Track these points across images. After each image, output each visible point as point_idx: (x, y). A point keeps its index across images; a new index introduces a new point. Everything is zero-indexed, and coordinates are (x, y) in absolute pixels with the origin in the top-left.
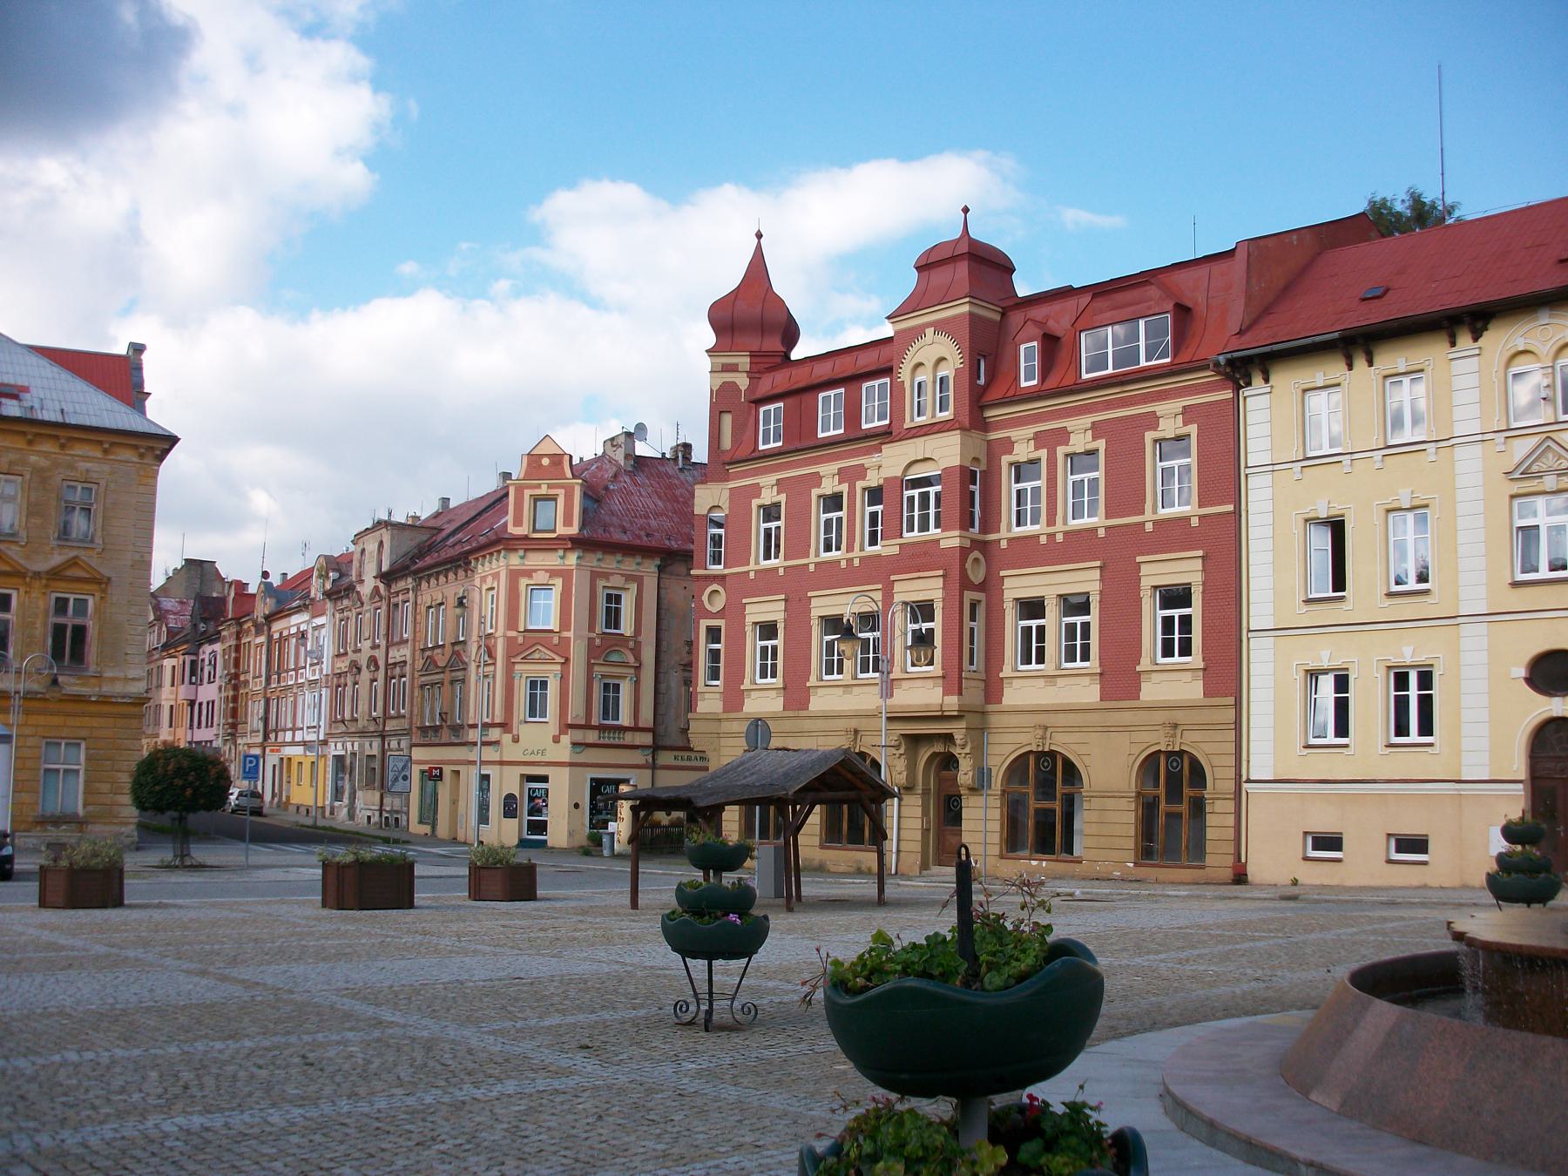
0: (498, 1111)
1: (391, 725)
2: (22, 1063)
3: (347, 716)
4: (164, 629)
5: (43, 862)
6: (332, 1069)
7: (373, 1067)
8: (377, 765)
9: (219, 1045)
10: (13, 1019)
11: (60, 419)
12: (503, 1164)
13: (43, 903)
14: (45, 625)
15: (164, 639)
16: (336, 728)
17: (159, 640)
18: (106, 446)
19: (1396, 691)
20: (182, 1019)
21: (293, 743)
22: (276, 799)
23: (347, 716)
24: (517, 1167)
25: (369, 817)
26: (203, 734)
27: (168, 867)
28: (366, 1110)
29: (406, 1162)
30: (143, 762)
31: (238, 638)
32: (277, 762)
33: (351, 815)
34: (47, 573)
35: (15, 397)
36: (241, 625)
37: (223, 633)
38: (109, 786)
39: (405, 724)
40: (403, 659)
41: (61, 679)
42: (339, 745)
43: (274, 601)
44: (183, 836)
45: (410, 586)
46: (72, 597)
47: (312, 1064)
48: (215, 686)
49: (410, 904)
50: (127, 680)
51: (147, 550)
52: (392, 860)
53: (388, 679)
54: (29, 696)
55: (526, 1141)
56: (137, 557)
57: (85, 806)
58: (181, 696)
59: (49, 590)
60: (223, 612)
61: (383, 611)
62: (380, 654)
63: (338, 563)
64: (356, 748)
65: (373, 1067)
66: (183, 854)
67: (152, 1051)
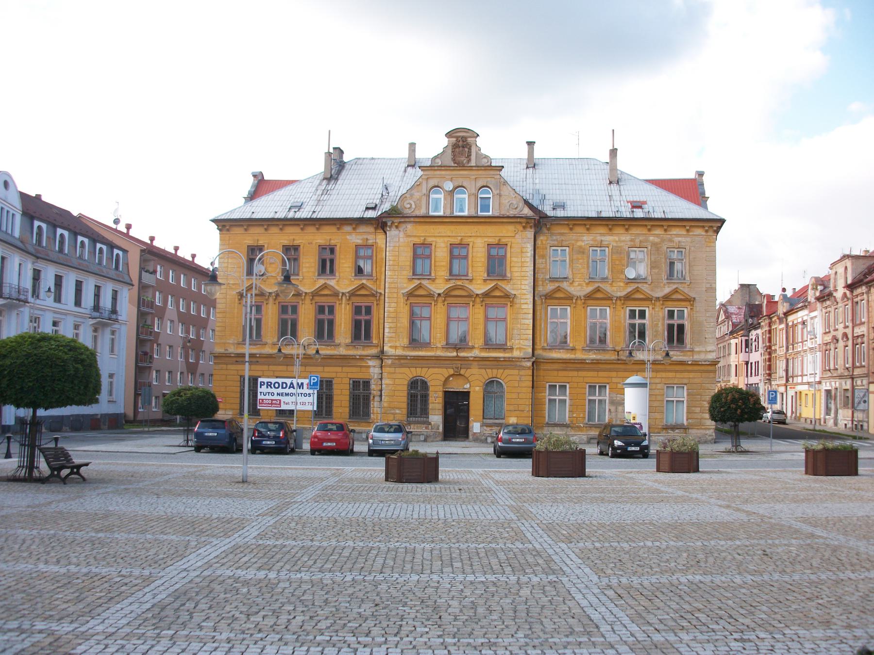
0: (860, 586)
1: (857, 372)
2: (625, 545)
3: (832, 367)
4: (730, 323)
5: (659, 449)
6: (776, 558)
7: (799, 559)
8: (849, 394)
9: (722, 543)
10: (627, 525)
11: (663, 217)
12: (851, 613)
13: (659, 470)
14: (663, 325)
15: (730, 329)
16: (826, 374)
17: (728, 329)
18: (688, 228)
19: (639, 310)
20: (709, 529)
21: (802, 383)
22: (794, 415)
23: (832, 367)
24: (858, 616)
25: (846, 425)
26: (753, 380)
27: (729, 452)
28: (787, 579)
29: (798, 607)
30: (714, 396)
31: (770, 326)
32: (794, 394)
33: (836, 424)
34: (663, 297)
35: (640, 207)
36: (771, 319)
37: (762, 324)
38: (699, 409)
39: (864, 371)
40: (862, 333)
41: (671, 353)
42: (828, 384)
43: (788, 304)
44: (736, 435)
45: (864, 291)
46: (676, 309)
47: (767, 555)
48: (759, 353)
49: (856, 473)
50: (706, 352)
51: (713, 281)
52: (845, 448)
53: (854, 345)
54: (655, 363)
55: (869, 603)
56: (708, 286)
57: (687, 420)
58: (741, 360)
59: (625, 306)
60: (761, 312)
61: (849, 306)
62: (849, 331)
63: (822, 281)
64: (837, 385)
65: (799, 559)
66: (737, 446)
67: (688, 544)
